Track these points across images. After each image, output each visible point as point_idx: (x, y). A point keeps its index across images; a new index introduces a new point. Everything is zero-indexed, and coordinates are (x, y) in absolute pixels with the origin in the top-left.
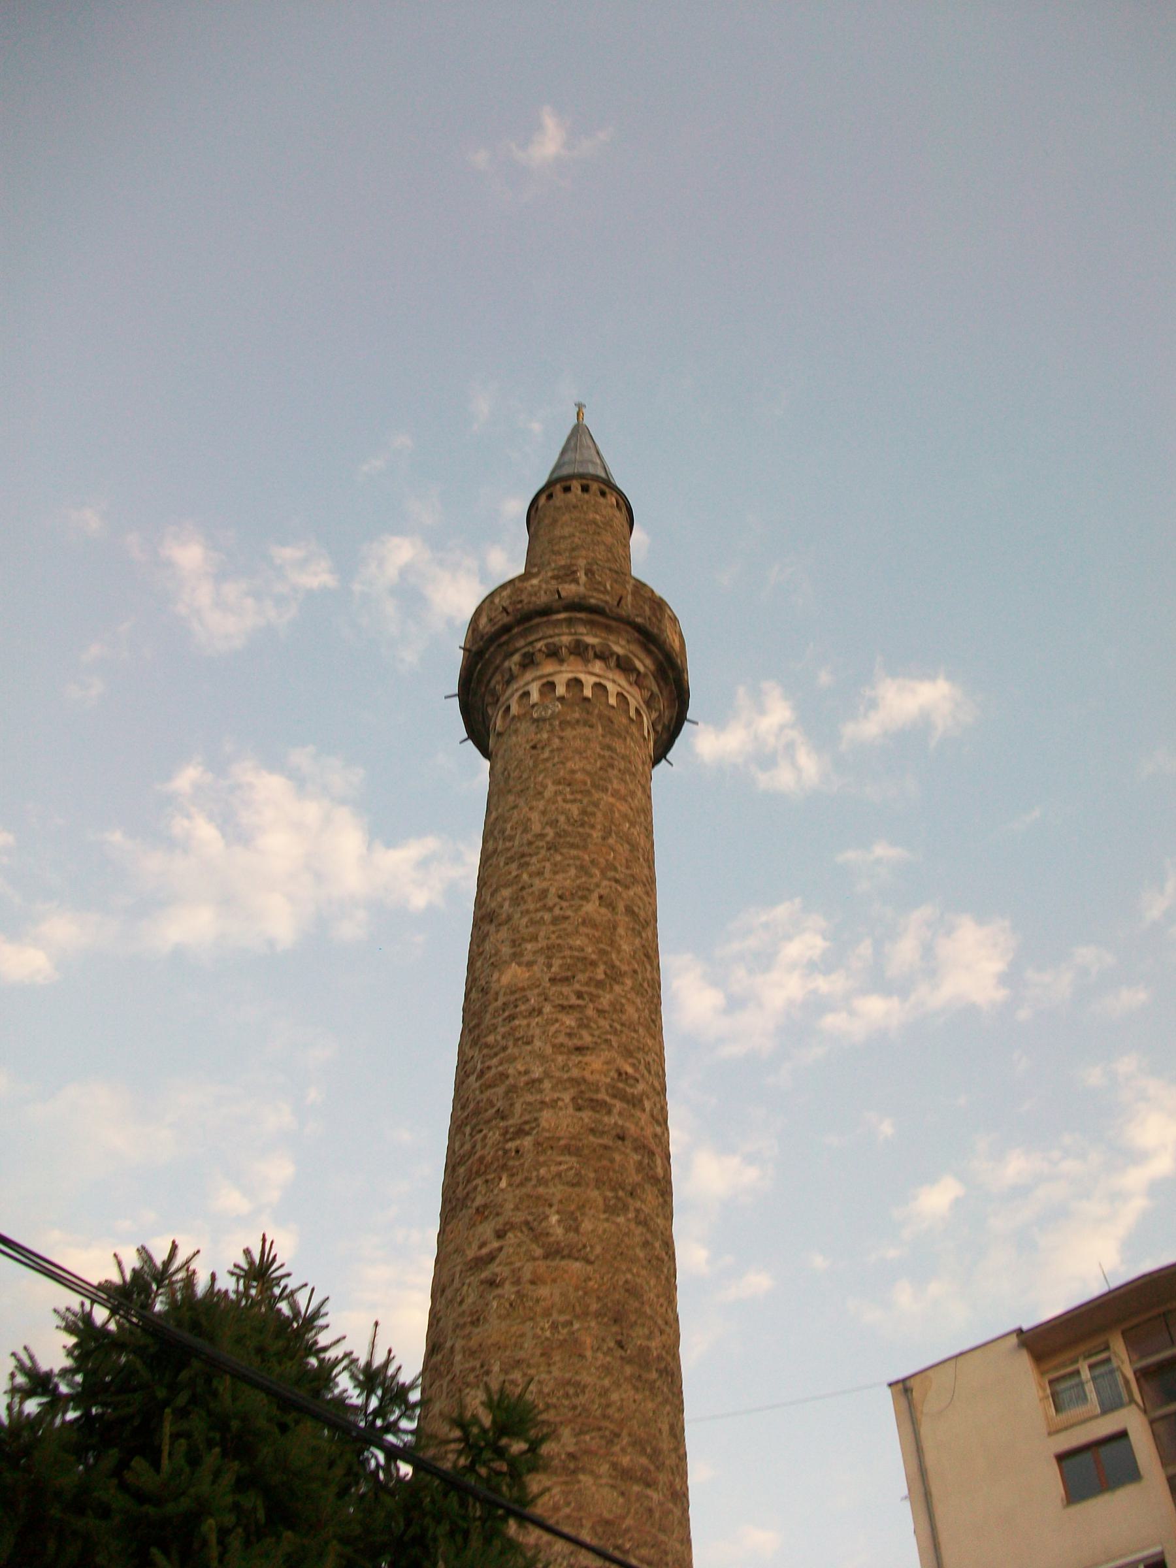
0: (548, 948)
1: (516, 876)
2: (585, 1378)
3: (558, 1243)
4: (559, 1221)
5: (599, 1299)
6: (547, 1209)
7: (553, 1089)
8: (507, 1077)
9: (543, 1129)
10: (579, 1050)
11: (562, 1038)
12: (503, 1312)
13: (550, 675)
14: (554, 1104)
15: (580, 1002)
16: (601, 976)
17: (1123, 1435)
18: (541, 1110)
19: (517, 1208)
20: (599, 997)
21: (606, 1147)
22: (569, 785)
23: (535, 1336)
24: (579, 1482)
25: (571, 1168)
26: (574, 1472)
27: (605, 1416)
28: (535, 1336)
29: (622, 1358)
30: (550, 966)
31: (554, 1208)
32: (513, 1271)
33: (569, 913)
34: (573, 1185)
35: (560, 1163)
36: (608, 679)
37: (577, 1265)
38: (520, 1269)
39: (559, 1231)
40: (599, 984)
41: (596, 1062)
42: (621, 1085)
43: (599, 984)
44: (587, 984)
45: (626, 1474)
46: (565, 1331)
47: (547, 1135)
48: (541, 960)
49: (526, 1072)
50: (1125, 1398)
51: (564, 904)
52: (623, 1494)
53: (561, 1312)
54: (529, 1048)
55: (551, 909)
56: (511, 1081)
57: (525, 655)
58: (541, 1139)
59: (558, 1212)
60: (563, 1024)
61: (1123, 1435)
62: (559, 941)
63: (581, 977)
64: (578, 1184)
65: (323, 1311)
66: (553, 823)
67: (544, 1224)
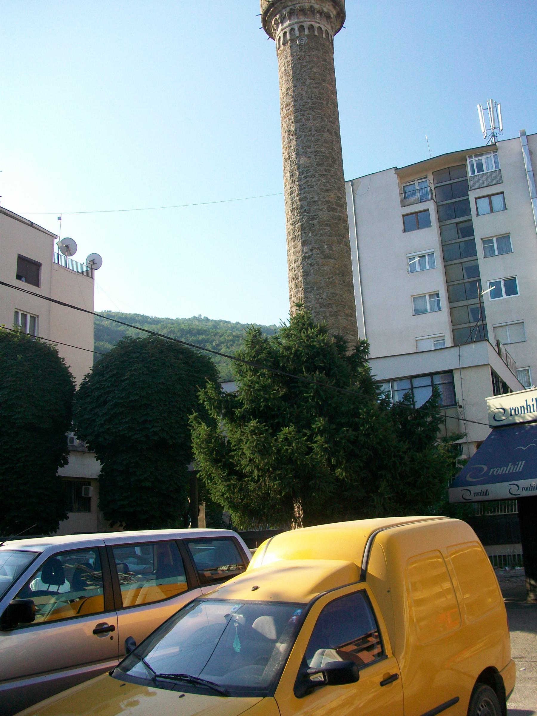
0: (315, 152)
1: (300, 119)
2: (337, 292)
3: (327, 254)
4: (327, 247)
5: (339, 270)
6: (324, 244)
7: (322, 204)
8: (307, 199)
9: (320, 218)
10: (327, 190)
11: (322, 187)
12: (315, 273)
13: (302, 22)
14: (321, 210)
15: (326, 173)
16: (331, 163)
17: (428, 210)
18: (319, 212)
19: (315, 243)
20: (330, 170)
21: (336, 223)
22: (314, 80)
23: (325, 281)
24: (338, 318)
25: (329, 231)
26: (337, 315)
27: (342, 301)
28: (325, 281)
29: (345, 285)
30: (316, 159)
31: (325, 244)
32: (316, 262)
33: (320, 138)
34: (330, 236)
35: (326, 229)
36: (322, 24)
37: (333, 260)
38: (318, 261)
39: (327, 250)
40: (330, 166)
41: (332, 195)
42: (338, 201)
43: (330, 166)
44: (327, 166)
45: (347, 315)
46: (331, 279)
47: (322, 220)
48: (313, 156)
49: (313, 198)
50: (430, 198)
51: (318, 134)
52: (347, 320)
53: (330, 274)
54: (313, 189)
55: (314, 136)
56: (308, 200)
57: (291, 9)
58: (320, 222)
59: (326, 245)
60: (322, 181)
61: (428, 210)
62: (318, 149)
63: (325, 163)
64: (331, 236)
65: (369, 361)
66: (310, 98)
67: (323, 249)
